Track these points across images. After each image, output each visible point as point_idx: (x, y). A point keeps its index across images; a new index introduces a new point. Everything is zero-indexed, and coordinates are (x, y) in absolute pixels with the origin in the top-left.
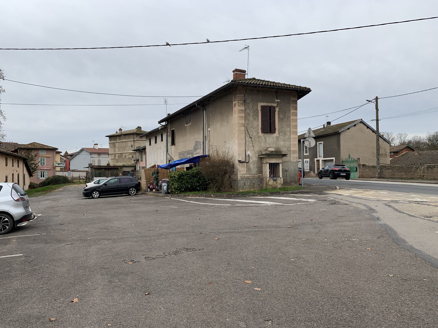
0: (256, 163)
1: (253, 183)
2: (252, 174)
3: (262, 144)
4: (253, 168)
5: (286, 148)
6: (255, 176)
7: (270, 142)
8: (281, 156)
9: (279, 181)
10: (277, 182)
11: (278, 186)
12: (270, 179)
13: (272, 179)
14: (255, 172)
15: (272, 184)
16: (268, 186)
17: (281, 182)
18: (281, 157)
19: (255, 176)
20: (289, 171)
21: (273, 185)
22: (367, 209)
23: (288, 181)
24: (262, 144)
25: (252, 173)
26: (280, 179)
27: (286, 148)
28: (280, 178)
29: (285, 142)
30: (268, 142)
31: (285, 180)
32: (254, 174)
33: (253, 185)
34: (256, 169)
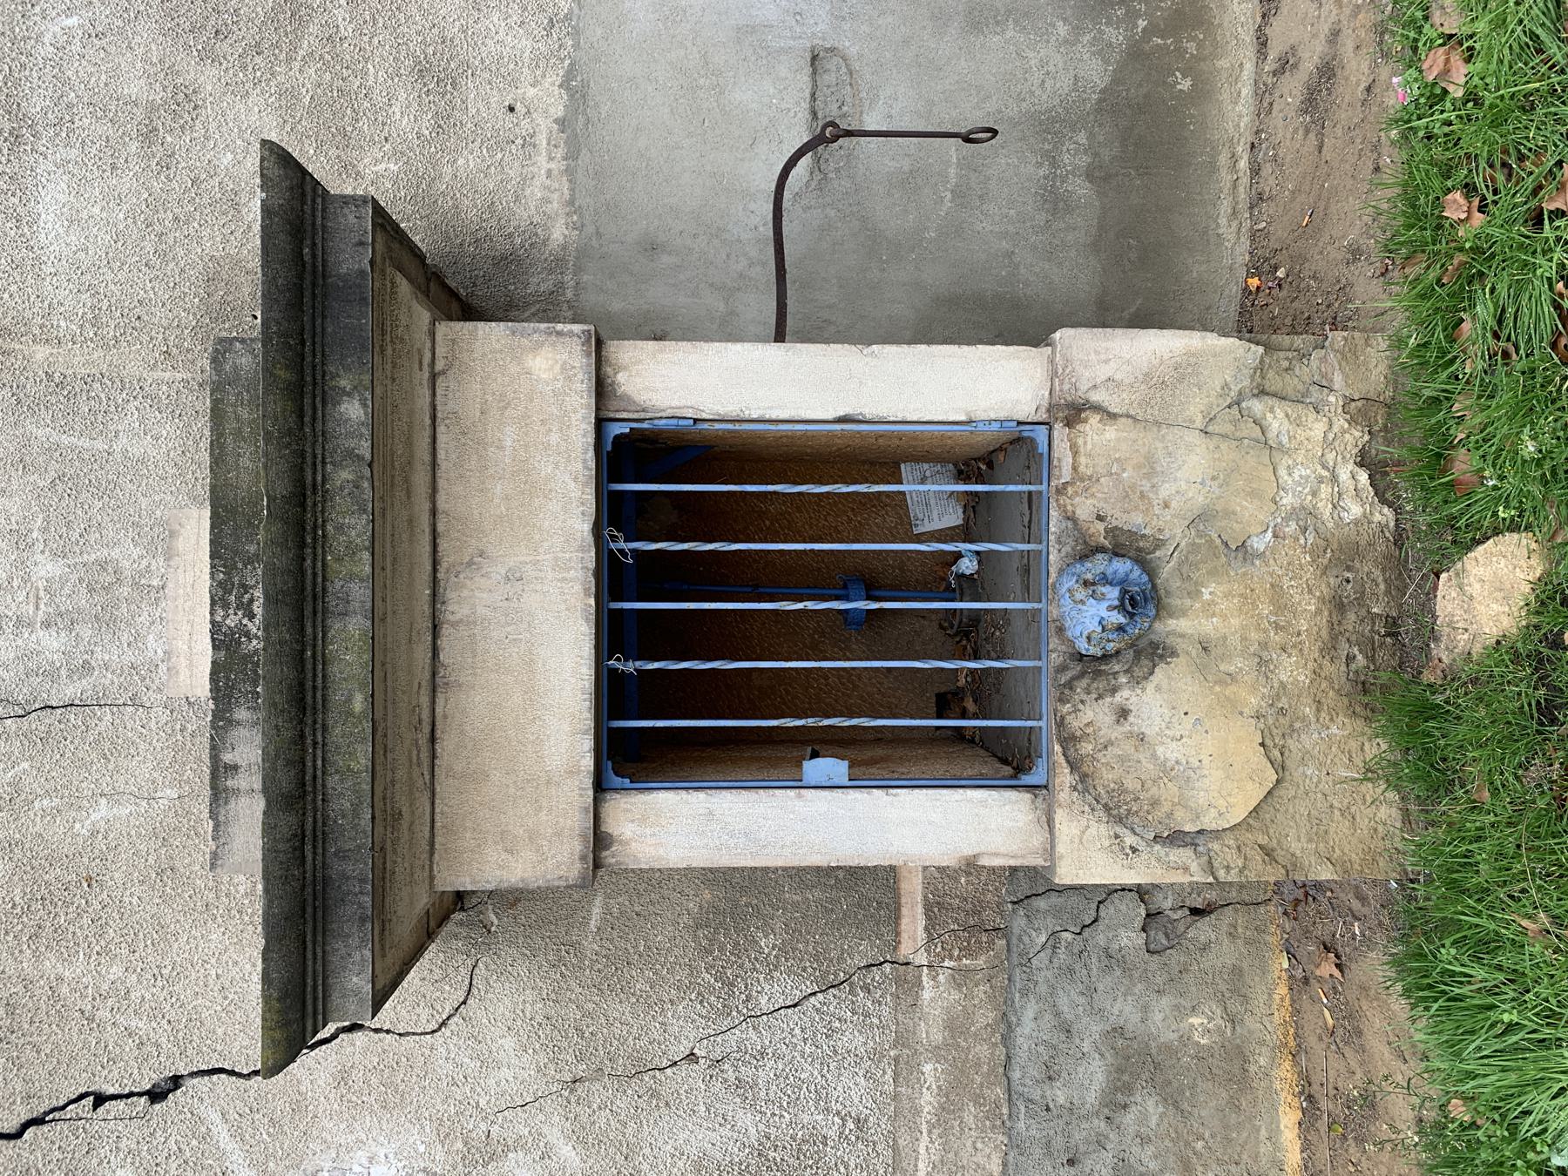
0: (619, 1009)
1: (1115, 1102)
2: (901, 1110)
3: (102, 811)
4: (732, 1106)
5: (208, 79)
6: (955, 1026)
7: (46, 568)
8: (353, 410)
9: (1150, 468)
10: (1200, 519)
11: (1306, 516)
12: (1084, 781)
13: (1093, 715)
14: (853, 1039)
15: (1233, 707)
16: (1296, 844)
17: (1195, 409)
18: (378, 424)
19: (938, 1037)
20: (820, 27)
21: (1292, 671)
22: (261, 682)
23: (1096, 73)
24: (102, 811)
25: (879, 1126)
26: (1094, 432)
27: (208, 79)
28: (1073, 412)
29: (36, 105)
30: (52, 643)
31: (1073, 157)
32: (905, 1070)
33: (1172, 1101)
34: (772, 992)
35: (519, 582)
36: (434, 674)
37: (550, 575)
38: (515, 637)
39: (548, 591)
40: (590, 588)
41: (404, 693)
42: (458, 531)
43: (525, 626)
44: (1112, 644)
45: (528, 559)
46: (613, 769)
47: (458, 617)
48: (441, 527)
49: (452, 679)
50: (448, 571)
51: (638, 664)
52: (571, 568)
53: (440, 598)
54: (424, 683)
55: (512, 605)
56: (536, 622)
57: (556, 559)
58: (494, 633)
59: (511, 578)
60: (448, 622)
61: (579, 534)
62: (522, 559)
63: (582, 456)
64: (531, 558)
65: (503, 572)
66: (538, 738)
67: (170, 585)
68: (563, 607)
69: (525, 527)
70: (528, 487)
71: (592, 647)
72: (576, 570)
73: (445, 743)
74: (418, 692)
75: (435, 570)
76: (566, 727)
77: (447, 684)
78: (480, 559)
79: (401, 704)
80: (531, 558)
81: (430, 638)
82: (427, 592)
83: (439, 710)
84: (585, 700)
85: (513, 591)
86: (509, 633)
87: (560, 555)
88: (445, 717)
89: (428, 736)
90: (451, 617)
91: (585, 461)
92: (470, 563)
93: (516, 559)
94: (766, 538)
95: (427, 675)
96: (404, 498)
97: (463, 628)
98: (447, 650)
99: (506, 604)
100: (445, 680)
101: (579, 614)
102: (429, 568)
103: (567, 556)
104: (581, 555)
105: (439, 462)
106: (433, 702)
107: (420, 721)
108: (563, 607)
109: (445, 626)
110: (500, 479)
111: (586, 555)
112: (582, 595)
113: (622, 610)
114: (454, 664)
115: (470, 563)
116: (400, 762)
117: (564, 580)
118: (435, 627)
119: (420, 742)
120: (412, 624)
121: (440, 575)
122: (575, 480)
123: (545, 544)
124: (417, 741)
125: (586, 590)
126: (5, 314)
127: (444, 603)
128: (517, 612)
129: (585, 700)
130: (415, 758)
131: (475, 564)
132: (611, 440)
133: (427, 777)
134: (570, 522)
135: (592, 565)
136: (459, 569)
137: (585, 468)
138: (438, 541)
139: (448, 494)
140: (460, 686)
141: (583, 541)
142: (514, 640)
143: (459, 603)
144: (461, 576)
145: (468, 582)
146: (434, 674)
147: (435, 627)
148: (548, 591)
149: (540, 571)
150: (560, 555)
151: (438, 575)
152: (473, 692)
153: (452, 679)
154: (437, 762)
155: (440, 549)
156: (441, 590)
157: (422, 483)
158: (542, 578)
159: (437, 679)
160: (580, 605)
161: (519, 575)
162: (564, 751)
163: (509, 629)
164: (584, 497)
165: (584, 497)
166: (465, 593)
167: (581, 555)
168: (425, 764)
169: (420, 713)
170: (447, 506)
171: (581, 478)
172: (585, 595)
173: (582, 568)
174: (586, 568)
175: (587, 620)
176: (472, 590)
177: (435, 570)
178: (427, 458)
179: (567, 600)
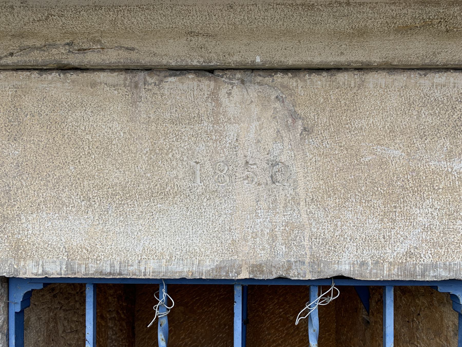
35: (269, 179)
36: (149, 69)
37: (279, 219)
38: (198, 173)
39: (257, 216)
40: (262, 272)
41: (113, 22)
42: (337, 100)
43: (212, 187)
45: (301, 191)
46: (32, 290)
47: (224, 100)
48: (342, 77)
49: (143, 93)
50: (283, 86)
51: (164, 322)
52: (289, 247)
53: (248, 76)
54: (134, 56)
55: (240, 170)
56: (217, 201)
57: (301, 227)
58: (202, 147)
59: (275, 169)
60: (217, 88)
61: (335, 259)
62: (301, 183)
63: (441, 263)
64: (303, 196)
65: (283, 158)
66: (63, 204)
68: (237, 236)
69: (344, 187)
70: (399, 191)
71: (184, 275)
72: (287, 254)
73: (59, 85)
74: (121, 47)
75: (286, 70)
76: (77, 241)
77: (136, 86)
78: (300, 128)
79: (95, 19)
80: (303, 196)
81: (195, 63)
82: (258, 60)
83: (102, 76)
84: (112, 266)
86: (202, 166)
87: (307, 234)
88: (94, 85)
89: (65, 62)
90: (223, 92)
91: (435, 266)
92: (294, 116)
93: (301, 174)
94: (305, 336)
95: (146, 60)
96: (400, 22)
97: (210, 107)
98: (180, 86)
99: (241, 162)
100: (141, 84)
101: (226, 257)
102: (291, 61)
103: (306, 243)
104: (307, 260)
105: (431, 75)
106: (112, 69)
107: (82, 50)
108: (237, 236)
109: (212, 84)
110: (408, 154)
111: (306, 268)
112: (252, 262)
113: (232, 301)
114: (162, 95)
115: (294, 116)
116: (10, 17)
117: (273, 238)
118: (211, 71)
119: (54, 51)
120: (213, 36)
121: (279, 78)
122: (409, 254)
123: (321, 213)
124: (54, 45)
125: (259, 267)
126: (115, 346)
127: (243, 82)
128: (230, 176)
129: (112, 266)
130: (29, 42)
131: (294, 121)
132: (452, 292)
133: (10, 61)
134: (352, 247)
135: (294, 275)
136: (286, 102)
137: (425, 266)
138: (325, 74)
139: (387, 86)
140: (134, 103)
141: (327, 264)
142: (194, 173)
143: (242, 102)
144: (278, 105)
145: (270, 112)
146: (149, 69)
147: (211, 71)
148: (257, 216)
150: (307, 234)
151: (279, 75)
152: (125, 119)
153: (143, 93)
154: (35, 74)
155: (315, 77)
156: (259, 79)
157: (411, 52)
158: (274, 209)
159: (142, 75)
160: (239, 258)
162: (45, 238)
163: (208, 165)
164: (386, 265)
165: (386, 265)
166: (255, 110)
167: (307, 260)
168: (26, 58)
169: (93, 50)
170: (371, 86)
171: (411, 261)
172: (253, 266)
173: (288, 261)
174: (290, 268)
175: (219, 268)
176: (259, 119)
177: (286, 70)
178: (441, 59)
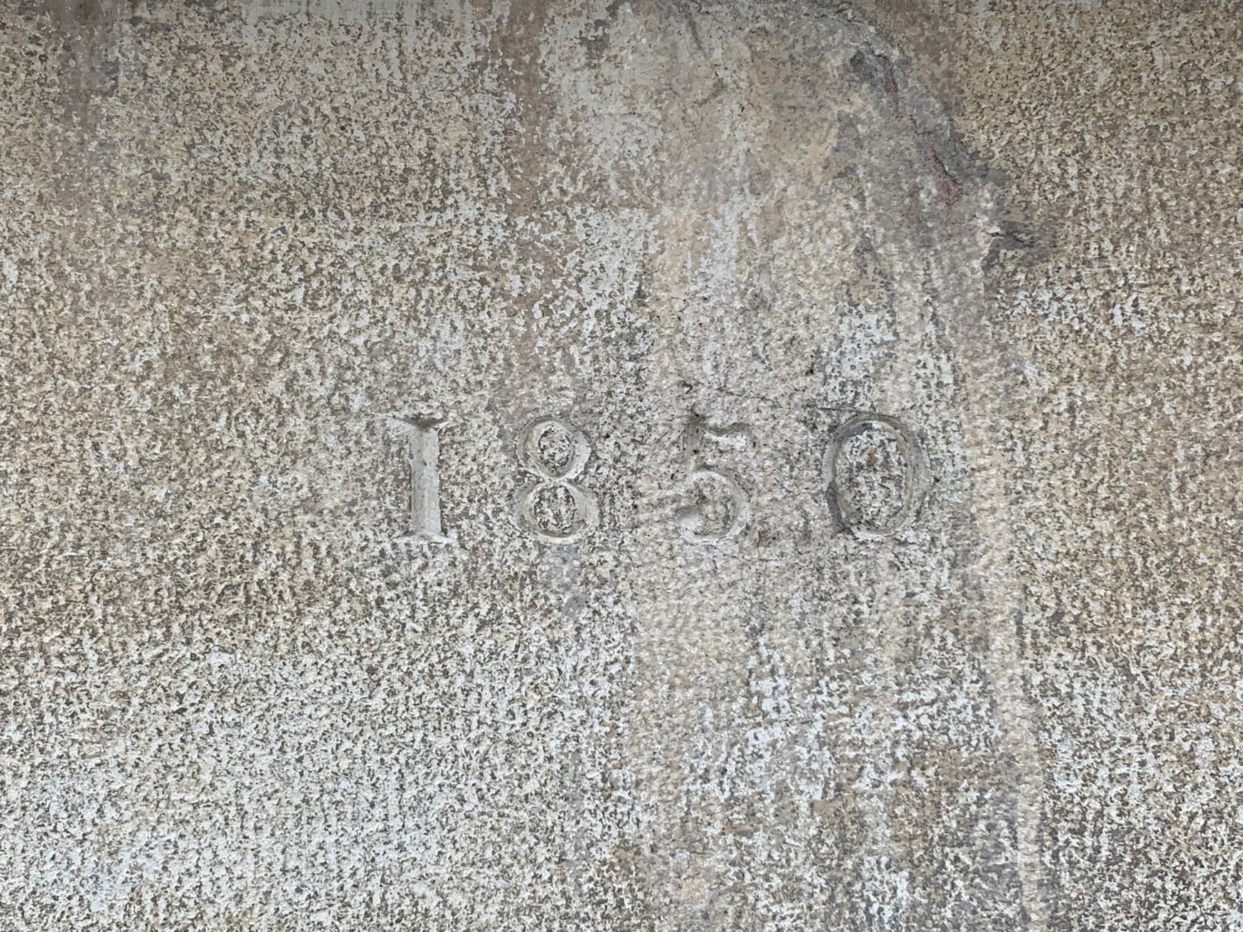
20: (421, 1)
35: (817, 510)
38: (430, 478)
44: (518, 283)
56: (536, 631)
59: (852, 454)
67: (475, 627)
78: (985, 230)
85: (759, 466)
86: (452, 441)
93: (994, 481)
114: (231, 55)
128: (604, 495)
131: (952, 190)
136: (910, 86)
142: (407, 479)
143: (665, 92)
149: (910, 658)
158: (849, 670)
161: (874, 502)
176: (759, 181)
179: (695, 846)
